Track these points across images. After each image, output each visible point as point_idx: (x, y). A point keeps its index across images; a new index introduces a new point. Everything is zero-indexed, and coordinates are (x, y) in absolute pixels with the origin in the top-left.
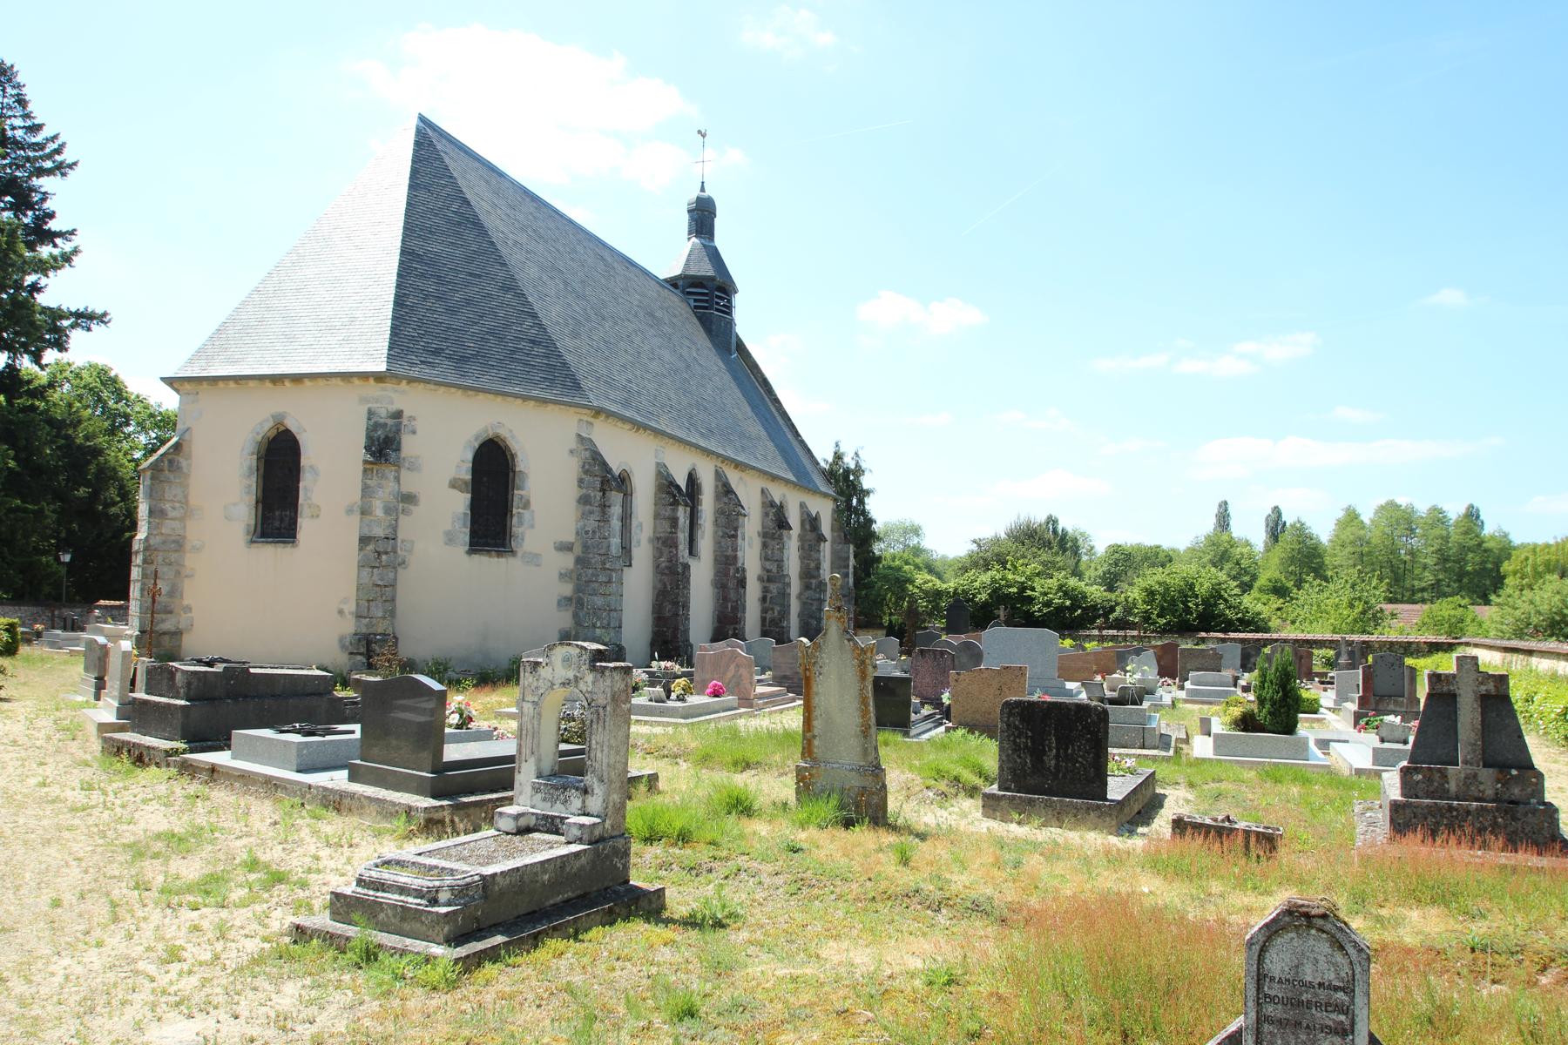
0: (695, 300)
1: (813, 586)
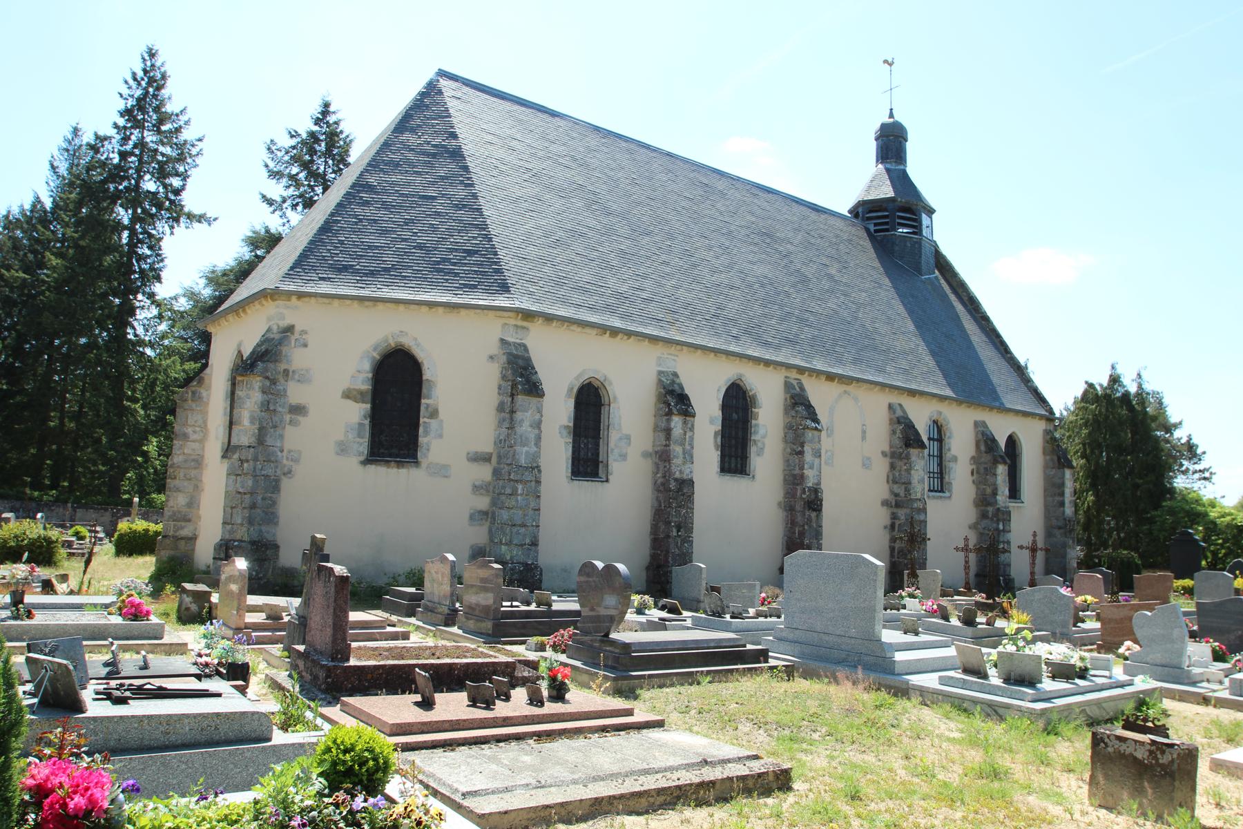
0: (875, 225)
1: (990, 514)
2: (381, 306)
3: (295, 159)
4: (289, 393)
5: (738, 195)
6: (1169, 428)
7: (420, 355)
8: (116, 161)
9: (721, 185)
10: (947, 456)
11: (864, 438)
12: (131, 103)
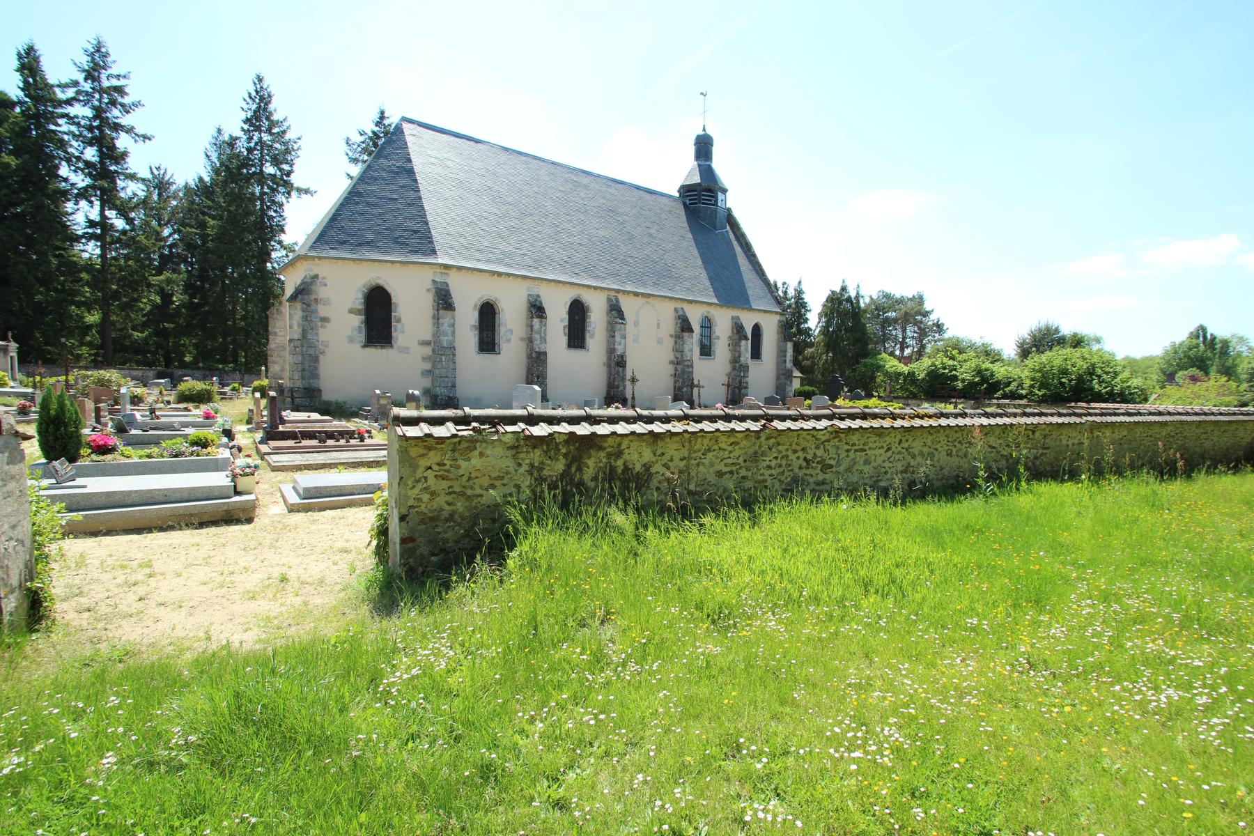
2: (365, 263)
3: (365, 150)
4: (319, 310)
5: (597, 187)
6: (926, 314)
7: (387, 287)
8: (245, 153)
9: (586, 180)
10: (714, 336)
11: (658, 327)
12: (250, 114)
